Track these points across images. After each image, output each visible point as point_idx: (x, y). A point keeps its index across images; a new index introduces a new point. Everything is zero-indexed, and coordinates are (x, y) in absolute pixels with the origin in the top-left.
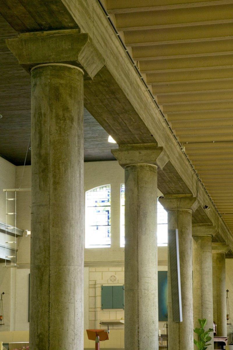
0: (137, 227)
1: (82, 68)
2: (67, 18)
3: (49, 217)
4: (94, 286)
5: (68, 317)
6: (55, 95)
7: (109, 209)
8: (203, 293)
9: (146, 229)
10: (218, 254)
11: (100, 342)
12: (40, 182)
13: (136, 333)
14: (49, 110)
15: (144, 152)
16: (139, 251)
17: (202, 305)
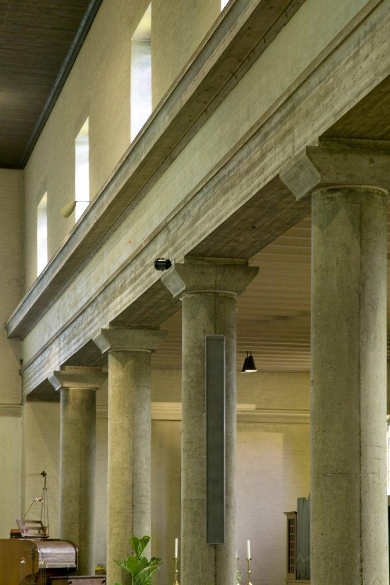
0: (358, 332)
8: (136, 478)
10: (83, 391)
16: (362, 386)
17: (133, 506)
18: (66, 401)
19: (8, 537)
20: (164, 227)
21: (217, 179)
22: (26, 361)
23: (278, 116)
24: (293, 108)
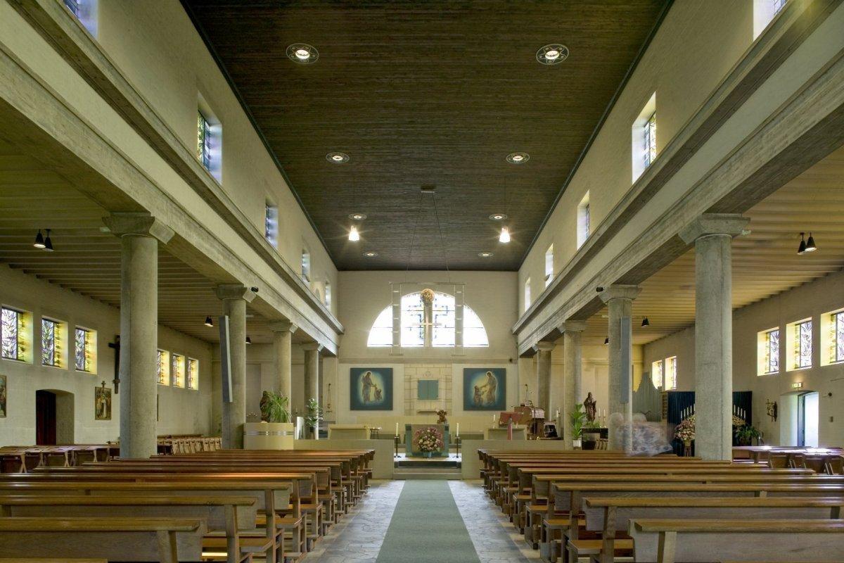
4: (410, 380)
7: (422, 313)
13: (719, 406)
18: (540, 356)
19: (155, 452)
20: (599, 275)
21: (633, 247)
22: (519, 342)
23: (673, 212)
24: (683, 206)
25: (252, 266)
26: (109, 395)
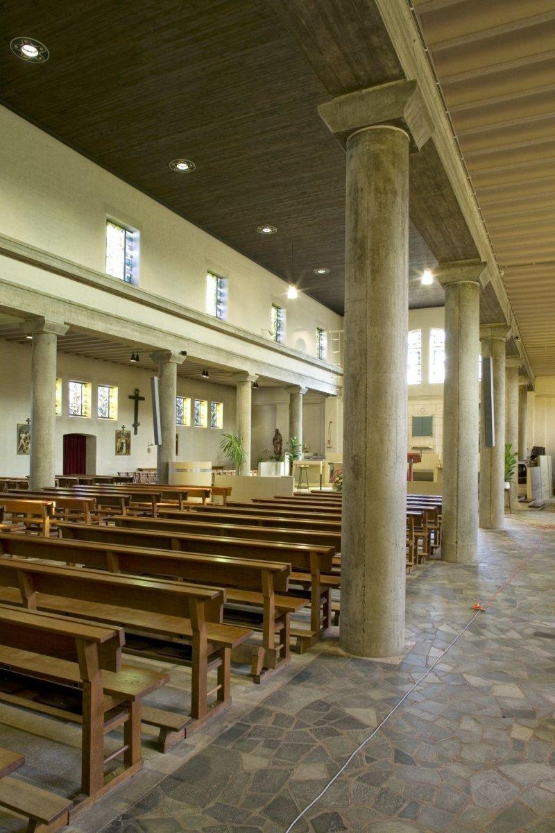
1: (407, 130)
2: (390, 60)
3: (366, 314)
5: (389, 435)
6: (375, 163)
7: (420, 350)
9: (468, 350)
11: (414, 464)
12: (355, 272)
14: (367, 182)
15: (466, 269)
25: (180, 333)
26: (128, 435)
